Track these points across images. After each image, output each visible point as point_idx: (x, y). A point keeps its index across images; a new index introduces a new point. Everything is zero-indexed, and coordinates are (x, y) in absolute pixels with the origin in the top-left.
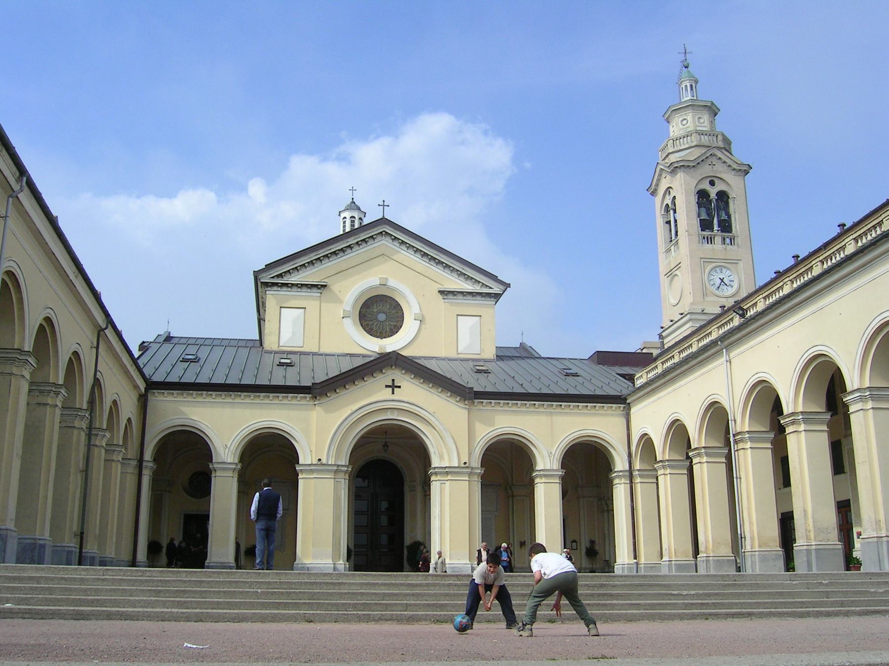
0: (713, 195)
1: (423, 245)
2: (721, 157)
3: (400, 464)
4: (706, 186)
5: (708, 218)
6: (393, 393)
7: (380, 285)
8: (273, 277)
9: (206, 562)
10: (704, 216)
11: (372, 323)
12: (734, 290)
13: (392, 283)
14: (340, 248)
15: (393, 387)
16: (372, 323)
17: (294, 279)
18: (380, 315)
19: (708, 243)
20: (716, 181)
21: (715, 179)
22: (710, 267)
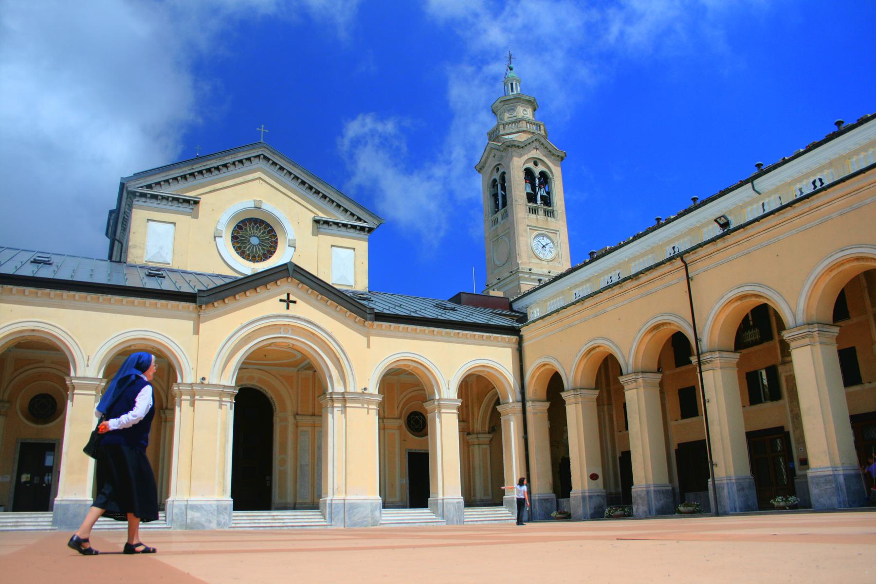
0: (537, 174)
1: (302, 173)
2: (544, 143)
3: (270, 394)
4: (531, 165)
5: (532, 192)
6: (288, 308)
7: (255, 207)
8: (142, 187)
9: (56, 499)
10: (530, 191)
11: (244, 245)
12: (553, 256)
13: (267, 206)
14: (215, 165)
15: (288, 302)
16: (244, 245)
17: (165, 191)
18: (253, 238)
19: (530, 212)
20: (539, 162)
21: (538, 161)
22: (536, 233)
